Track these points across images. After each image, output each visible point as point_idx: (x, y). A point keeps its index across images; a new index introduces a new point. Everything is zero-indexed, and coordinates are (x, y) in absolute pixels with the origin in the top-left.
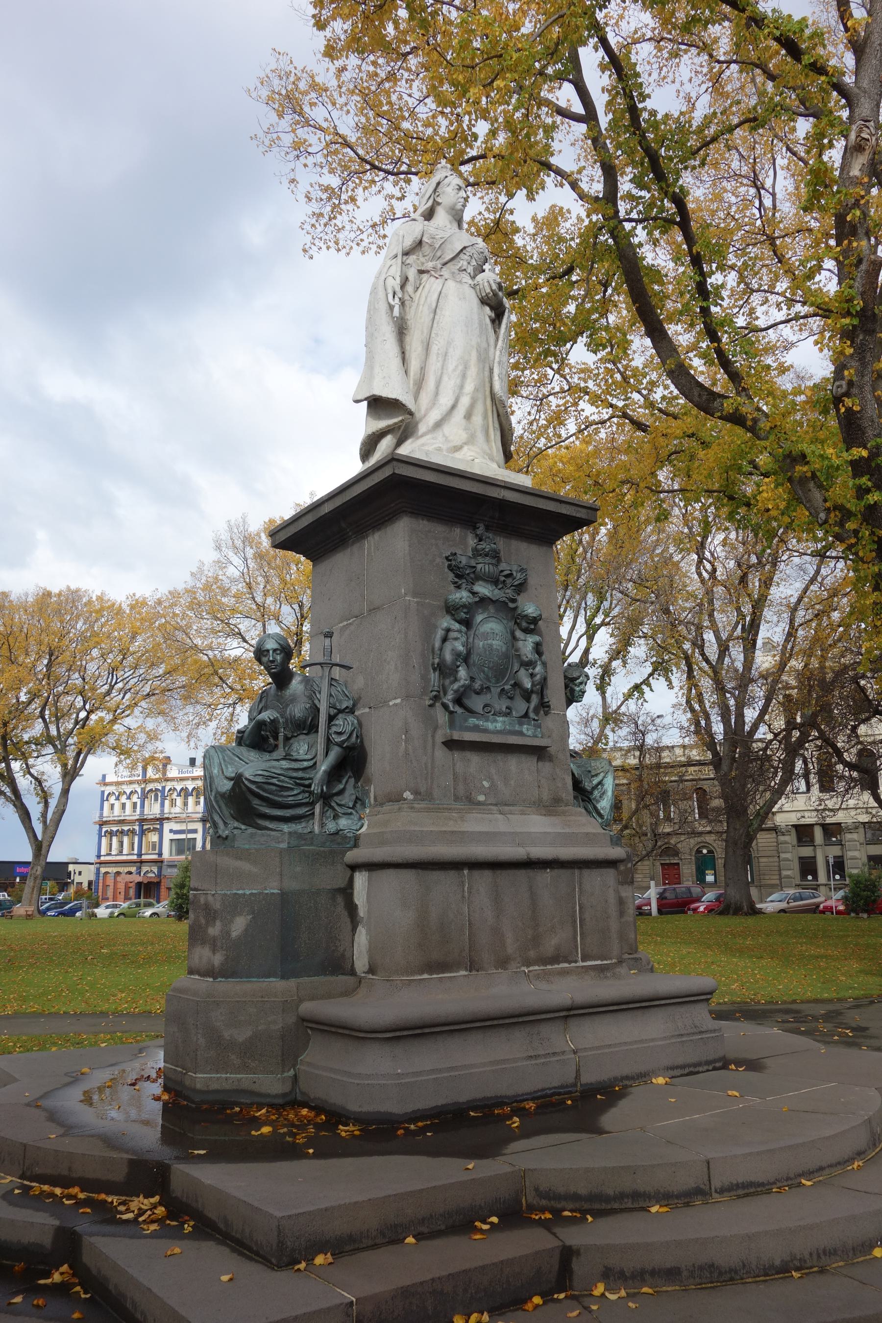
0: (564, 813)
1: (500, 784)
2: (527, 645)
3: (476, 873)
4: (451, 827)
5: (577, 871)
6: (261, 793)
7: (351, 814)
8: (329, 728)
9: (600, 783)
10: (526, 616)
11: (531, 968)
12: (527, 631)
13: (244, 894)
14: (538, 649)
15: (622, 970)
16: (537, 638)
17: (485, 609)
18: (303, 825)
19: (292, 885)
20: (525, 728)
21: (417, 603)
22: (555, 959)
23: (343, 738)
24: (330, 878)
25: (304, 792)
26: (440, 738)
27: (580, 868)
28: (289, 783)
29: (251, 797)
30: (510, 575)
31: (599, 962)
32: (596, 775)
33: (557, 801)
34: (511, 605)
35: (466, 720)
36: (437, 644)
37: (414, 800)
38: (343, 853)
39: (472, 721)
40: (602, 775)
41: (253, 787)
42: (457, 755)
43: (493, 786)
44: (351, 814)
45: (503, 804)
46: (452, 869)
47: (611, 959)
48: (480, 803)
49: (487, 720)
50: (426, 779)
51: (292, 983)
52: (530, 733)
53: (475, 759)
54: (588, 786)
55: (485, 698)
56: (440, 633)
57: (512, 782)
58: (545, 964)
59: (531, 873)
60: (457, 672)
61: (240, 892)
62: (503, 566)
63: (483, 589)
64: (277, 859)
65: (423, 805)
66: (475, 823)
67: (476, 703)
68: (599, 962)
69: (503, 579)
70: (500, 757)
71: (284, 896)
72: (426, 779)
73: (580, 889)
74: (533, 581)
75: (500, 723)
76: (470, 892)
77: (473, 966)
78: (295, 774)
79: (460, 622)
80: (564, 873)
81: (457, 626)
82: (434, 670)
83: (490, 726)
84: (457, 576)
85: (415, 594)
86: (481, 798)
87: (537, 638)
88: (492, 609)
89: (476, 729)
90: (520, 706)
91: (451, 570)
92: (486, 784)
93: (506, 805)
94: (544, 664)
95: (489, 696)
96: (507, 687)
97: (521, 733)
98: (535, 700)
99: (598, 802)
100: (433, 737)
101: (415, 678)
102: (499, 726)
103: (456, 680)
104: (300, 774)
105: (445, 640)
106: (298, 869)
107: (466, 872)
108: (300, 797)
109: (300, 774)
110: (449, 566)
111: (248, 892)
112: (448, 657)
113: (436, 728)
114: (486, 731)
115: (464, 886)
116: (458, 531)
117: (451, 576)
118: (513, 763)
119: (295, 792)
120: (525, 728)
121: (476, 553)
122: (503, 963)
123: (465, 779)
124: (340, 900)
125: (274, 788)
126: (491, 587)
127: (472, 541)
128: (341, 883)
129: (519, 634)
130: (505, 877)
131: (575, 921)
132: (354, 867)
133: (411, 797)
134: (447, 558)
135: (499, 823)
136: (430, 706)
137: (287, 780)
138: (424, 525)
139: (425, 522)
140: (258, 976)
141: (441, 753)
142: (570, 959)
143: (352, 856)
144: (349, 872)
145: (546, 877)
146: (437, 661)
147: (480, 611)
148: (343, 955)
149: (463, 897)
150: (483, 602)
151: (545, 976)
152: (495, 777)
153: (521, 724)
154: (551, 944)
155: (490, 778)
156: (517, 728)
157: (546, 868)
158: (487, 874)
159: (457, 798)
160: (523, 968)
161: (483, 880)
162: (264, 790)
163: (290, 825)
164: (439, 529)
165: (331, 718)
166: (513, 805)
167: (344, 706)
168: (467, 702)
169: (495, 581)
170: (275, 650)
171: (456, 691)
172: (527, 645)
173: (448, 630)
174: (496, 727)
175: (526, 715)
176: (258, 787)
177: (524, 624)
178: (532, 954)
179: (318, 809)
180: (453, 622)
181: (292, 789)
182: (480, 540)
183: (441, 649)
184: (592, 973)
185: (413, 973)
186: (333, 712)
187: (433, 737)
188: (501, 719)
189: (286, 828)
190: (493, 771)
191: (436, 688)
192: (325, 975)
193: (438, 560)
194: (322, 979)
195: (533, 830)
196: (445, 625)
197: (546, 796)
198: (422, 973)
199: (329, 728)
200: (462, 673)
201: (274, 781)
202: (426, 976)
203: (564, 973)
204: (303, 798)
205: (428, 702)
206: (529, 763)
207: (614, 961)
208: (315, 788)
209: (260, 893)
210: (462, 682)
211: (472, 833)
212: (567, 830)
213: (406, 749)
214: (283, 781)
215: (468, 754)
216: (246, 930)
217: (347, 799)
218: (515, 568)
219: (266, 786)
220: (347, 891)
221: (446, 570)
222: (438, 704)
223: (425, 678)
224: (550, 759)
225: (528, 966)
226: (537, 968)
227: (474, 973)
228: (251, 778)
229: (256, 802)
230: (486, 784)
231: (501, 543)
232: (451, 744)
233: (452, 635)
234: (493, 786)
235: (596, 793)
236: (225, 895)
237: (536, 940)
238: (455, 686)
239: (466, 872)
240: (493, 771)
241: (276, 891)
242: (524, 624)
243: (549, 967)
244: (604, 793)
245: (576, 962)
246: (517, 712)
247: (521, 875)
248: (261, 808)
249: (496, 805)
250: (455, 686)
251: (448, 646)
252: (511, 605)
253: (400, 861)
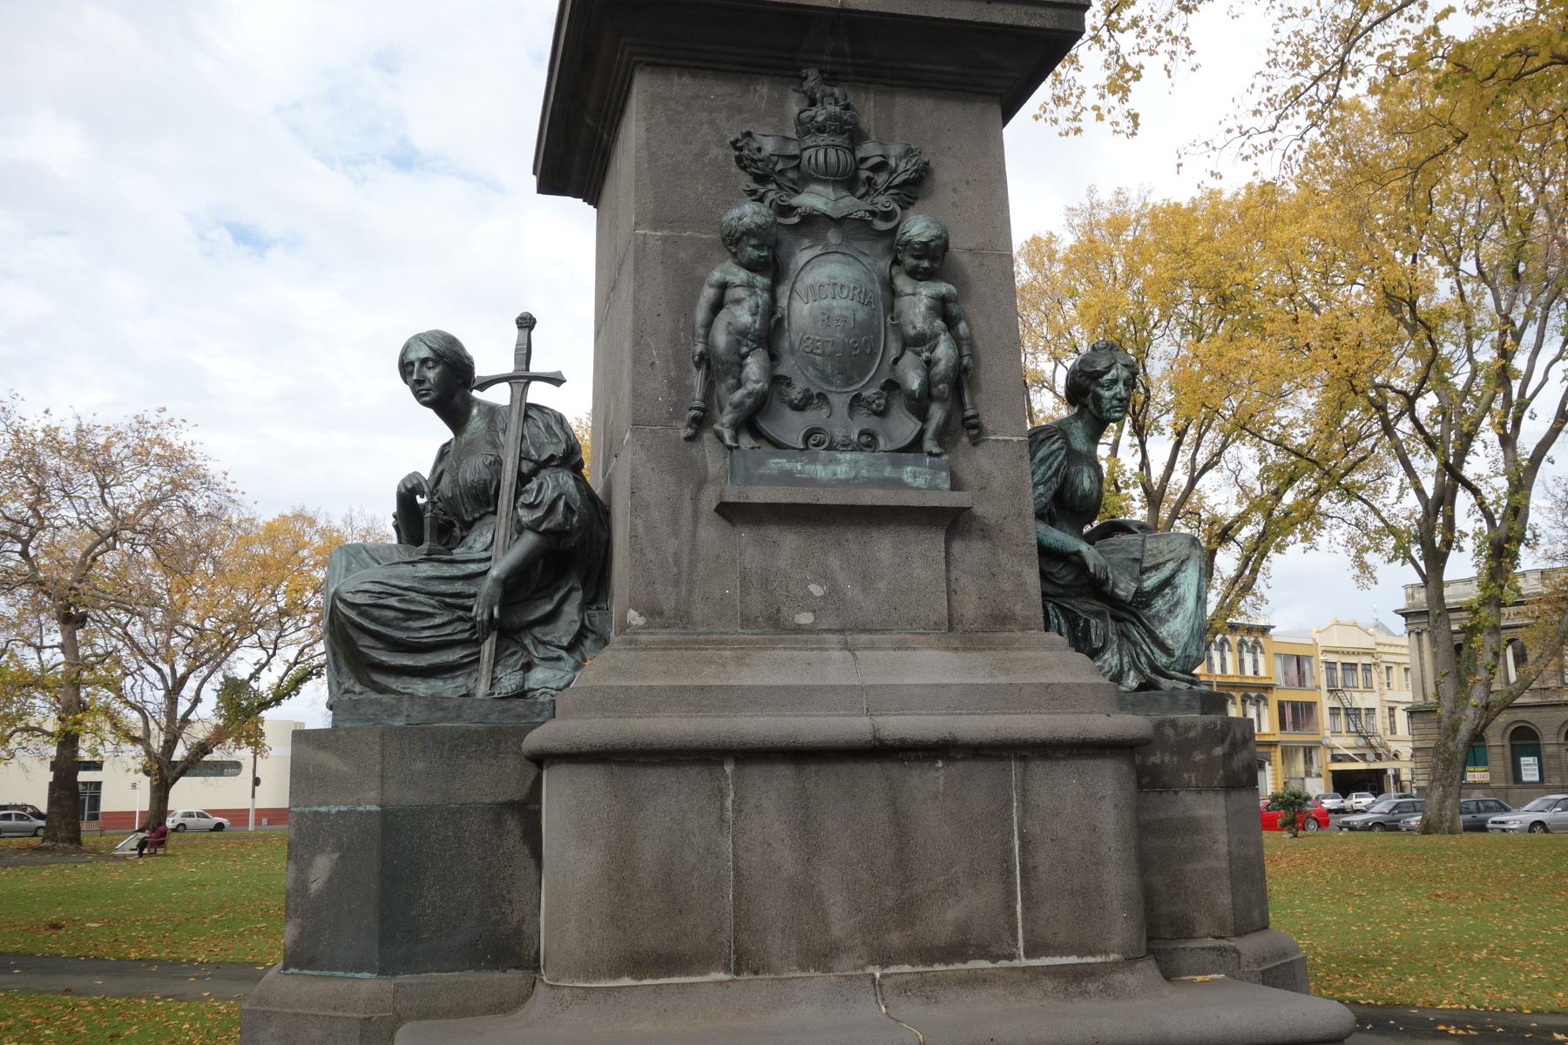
0: (1007, 645)
1: (851, 590)
2: (917, 302)
3: (755, 773)
4: (709, 677)
5: (1015, 767)
6: (366, 623)
7: (559, 659)
8: (518, 494)
9: (1168, 582)
10: (908, 242)
11: (893, 969)
12: (916, 274)
13: (328, 814)
14: (944, 310)
15: (1131, 979)
16: (943, 288)
17: (818, 239)
18: (460, 681)
19: (410, 797)
20: (907, 473)
21: (665, 239)
22: (957, 951)
23: (539, 513)
24: (490, 782)
25: (460, 619)
26: (709, 500)
27: (1024, 759)
28: (423, 604)
29: (354, 633)
30: (881, 166)
31: (1073, 960)
32: (1157, 567)
33: (1000, 620)
34: (881, 225)
35: (761, 463)
36: (701, 315)
37: (647, 626)
38: (521, 733)
39: (777, 463)
40: (1170, 566)
41: (352, 614)
42: (745, 535)
43: (834, 594)
44: (559, 659)
45: (854, 630)
46: (693, 763)
47: (1106, 952)
48: (800, 629)
49: (813, 461)
50: (677, 584)
51: (388, 984)
52: (920, 482)
53: (790, 543)
54: (1125, 588)
55: (813, 417)
56: (708, 294)
57: (882, 585)
58: (929, 959)
59: (895, 770)
60: (741, 367)
61: (323, 809)
62: (870, 150)
63: (816, 199)
64: (377, 748)
65: (662, 635)
66: (771, 668)
67: (791, 427)
68: (1073, 960)
69: (864, 174)
70: (852, 538)
71: (389, 818)
72: (677, 584)
73: (1024, 803)
74: (945, 174)
75: (844, 465)
76: (738, 810)
77: (743, 962)
78: (443, 588)
79: (751, 266)
80: (984, 772)
81: (742, 275)
82: (698, 365)
83: (820, 471)
84: (758, 179)
85: (657, 224)
86: (805, 618)
87: (943, 288)
88: (833, 236)
89: (787, 478)
90: (904, 427)
91: (744, 168)
92: (816, 590)
93: (864, 631)
94: (957, 341)
95: (824, 412)
96: (868, 393)
97: (898, 484)
98: (937, 413)
99: (1163, 621)
100: (695, 500)
101: (657, 385)
102: (842, 471)
103: (739, 385)
104: (458, 587)
105: (717, 306)
106: (419, 766)
107: (729, 768)
108: (449, 630)
109: (458, 587)
110: (739, 160)
111: (334, 810)
112: (721, 339)
113: (701, 484)
114: (811, 482)
115: (723, 797)
116: (763, 91)
117: (746, 181)
118: (884, 546)
119: (437, 621)
120: (907, 473)
121: (806, 128)
122: (820, 956)
123: (765, 582)
124: (512, 824)
125: (392, 614)
126: (829, 191)
127: (794, 105)
128: (514, 791)
129: (903, 283)
130: (824, 781)
131: (1009, 872)
132: (541, 760)
133: (640, 621)
134: (734, 144)
135: (833, 667)
136: (688, 439)
137: (422, 598)
138: (682, 86)
139: (686, 79)
140: (345, 968)
141: (711, 533)
142: (994, 950)
143: (536, 739)
144: (532, 771)
145: (939, 775)
146: (699, 348)
147: (806, 242)
148: (518, 931)
149: (722, 820)
150: (812, 223)
151: (925, 989)
152: (840, 576)
153: (897, 465)
154: (945, 918)
155: (825, 577)
156: (888, 472)
157: (935, 759)
158: (783, 774)
159: (747, 621)
160: (870, 969)
161: (771, 790)
162: (374, 619)
163: (432, 682)
164: (719, 91)
165: (523, 479)
166: (882, 631)
167: (545, 456)
168: (766, 426)
169: (847, 181)
170: (424, 361)
171: (736, 406)
172: (917, 302)
173: (723, 287)
174: (836, 474)
175: (915, 446)
176: (360, 614)
177: (910, 261)
178: (895, 939)
179: (487, 648)
180: (735, 269)
181: (431, 615)
182: (813, 103)
183: (709, 325)
184: (1049, 984)
185: (597, 974)
186: (526, 467)
187: (695, 500)
188: (848, 456)
189: (421, 687)
190: (834, 563)
191: (697, 403)
192: (477, 968)
193: (715, 152)
194: (471, 976)
195: (908, 681)
196: (716, 275)
197: (970, 608)
198: (619, 975)
199: (518, 494)
200: (754, 367)
201: (393, 602)
202: (626, 981)
203: (973, 981)
204: (459, 631)
205: (684, 432)
206: (927, 546)
207: (1112, 957)
208: (479, 612)
209: (351, 812)
210: (750, 386)
211: (750, 688)
212: (1002, 679)
213: (633, 528)
214: (411, 601)
215: (773, 532)
216: (330, 880)
217: (564, 629)
218: (895, 150)
219: (376, 612)
220: (527, 812)
221: (734, 169)
222: (707, 436)
223: (678, 385)
224: (985, 533)
225: (884, 965)
226: (907, 968)
227: (745, 976)
228: (350, 598)
229: (364, 642)
230: (816, 590)
231: (869, 109)
232: (730, 512)
233: (732, 294)
234: (834, 594)
235: (1159, 604)
236: (302, 813)
237: (906, 911)
238: (738, 395)
239: (729, 768)
240: (834, 563)
241: (374, 808)
242: (910, 261)
243: (939, 967)
244: (1176, 604)
245: (1011, 957)
246: (889, 437)
247: (871, 775)
248: (373, 653)
249: (841, 631)
250: (738, 395)
251: (723, 318)
252: (881, 225)
253: (566, 749)
